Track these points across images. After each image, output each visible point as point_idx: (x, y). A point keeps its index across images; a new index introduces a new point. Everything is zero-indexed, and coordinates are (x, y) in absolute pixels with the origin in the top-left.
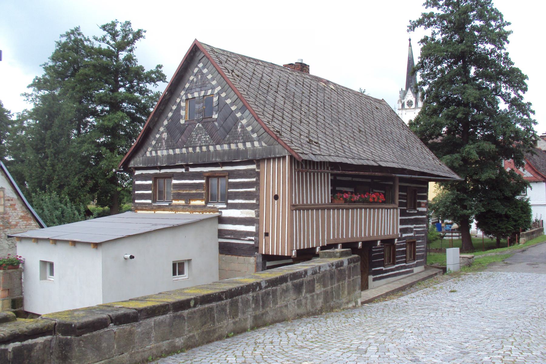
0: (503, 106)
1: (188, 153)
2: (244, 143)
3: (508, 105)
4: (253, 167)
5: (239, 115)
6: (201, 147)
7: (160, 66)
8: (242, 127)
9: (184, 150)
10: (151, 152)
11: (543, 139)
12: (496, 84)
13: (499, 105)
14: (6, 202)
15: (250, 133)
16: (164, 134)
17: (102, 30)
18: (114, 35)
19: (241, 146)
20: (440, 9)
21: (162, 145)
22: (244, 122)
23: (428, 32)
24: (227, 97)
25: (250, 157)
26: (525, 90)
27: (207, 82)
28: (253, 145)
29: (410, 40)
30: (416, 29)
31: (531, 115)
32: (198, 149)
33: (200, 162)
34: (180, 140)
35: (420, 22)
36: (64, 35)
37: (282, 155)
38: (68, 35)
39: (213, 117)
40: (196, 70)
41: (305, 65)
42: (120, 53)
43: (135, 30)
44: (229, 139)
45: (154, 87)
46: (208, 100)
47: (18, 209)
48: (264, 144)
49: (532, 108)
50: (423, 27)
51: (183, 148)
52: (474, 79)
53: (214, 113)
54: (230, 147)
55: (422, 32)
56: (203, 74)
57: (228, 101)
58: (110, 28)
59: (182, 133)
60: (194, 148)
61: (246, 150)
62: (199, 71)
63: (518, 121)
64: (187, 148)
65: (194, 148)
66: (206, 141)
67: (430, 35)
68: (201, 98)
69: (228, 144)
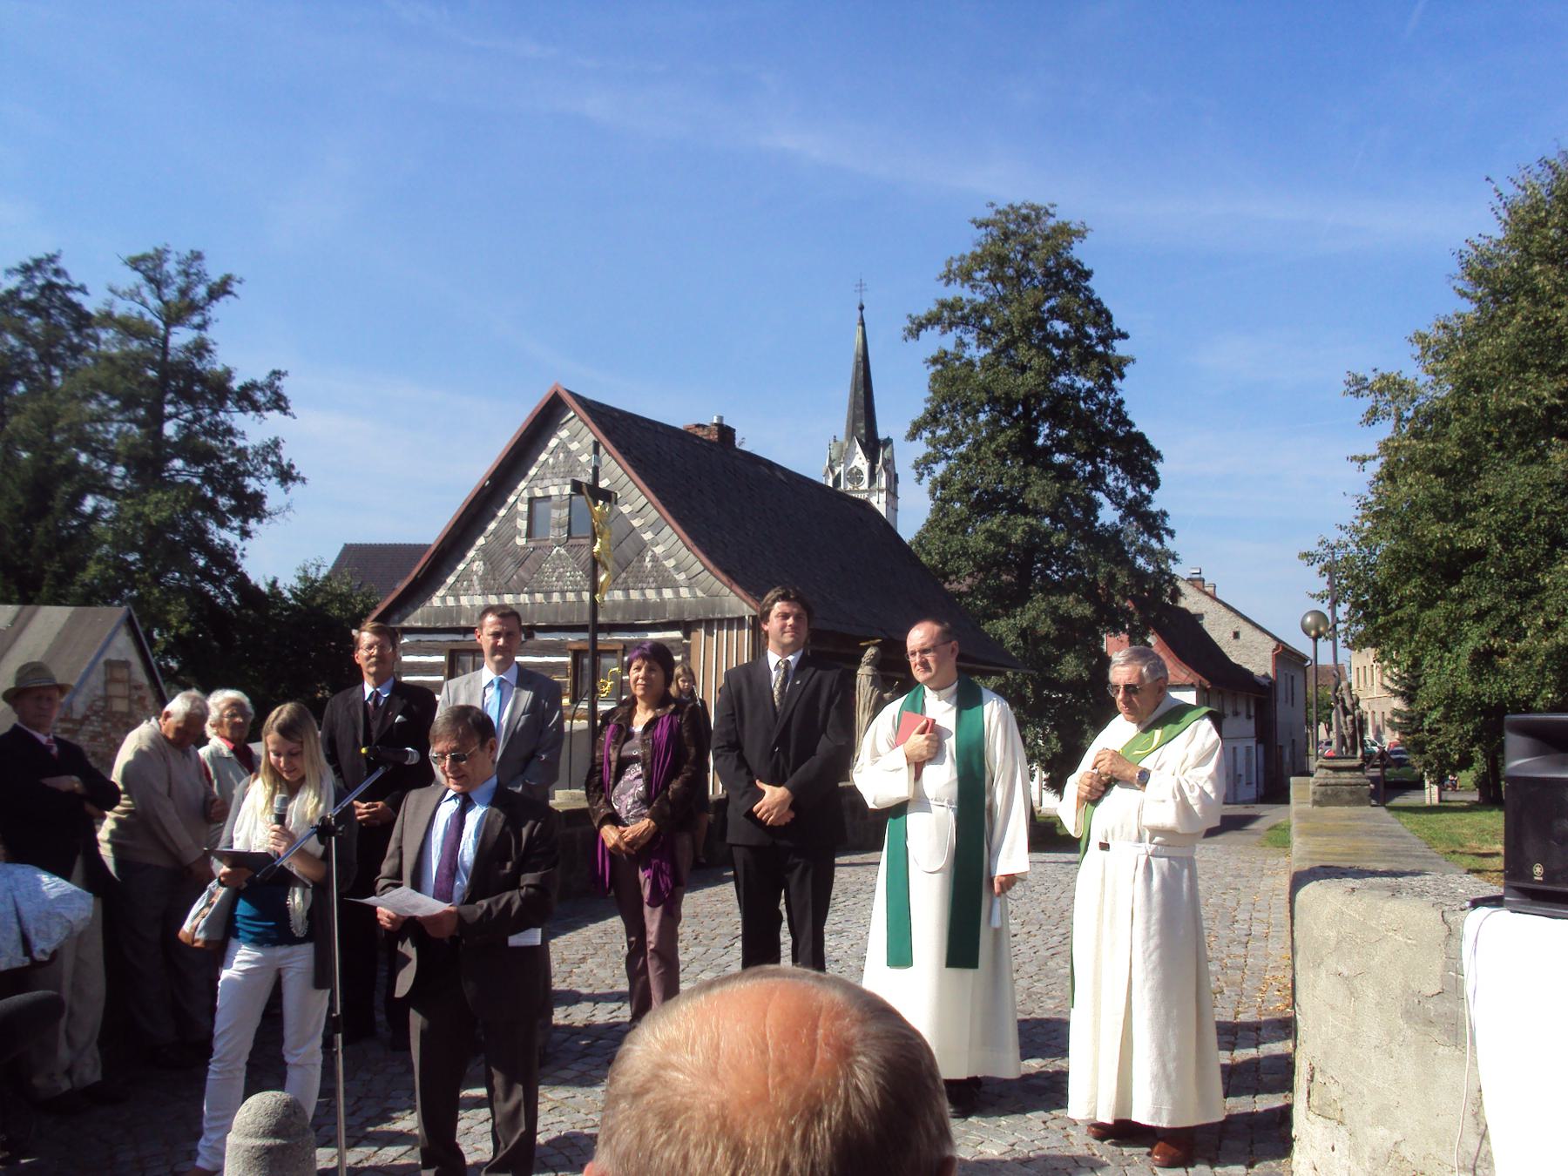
0: (1108, 515)
1: (533, 603)
2: (659, 589)
3: (1120, 512)
4: (677, 634)
5: (648, 536)
6: (563, 592)
7: (277, 374)
8: (655, 559)
9: (524, 598)
10: (443, 598)
11: (1194, 585)
12: (1094, 464)
13: (1100, 513)
14: (133, 691)
15: (673, 572)
16: (477, 563)
17: (128, 269)
18: (157, 283)
19: (651, 595)
21: (471, 585)
22: (659, 550)
23: (948, 342)
25: (669, 617)
26: (1154, 484)
27: (579, 469)
28: (677, 593)
29: (862, 308)
30: (923, 333)
31: (1166, 538)
32: (556, 597)
33: (561, 621)
34: (515, 577)
35: (932, 320)
36: (17, 270)
37: (736, 616)
38: (26, 270)
40: (553, 443)
42: (173, 329)
43: (215, 277)
45: (256, 422)
47: (150, 708)
48: (699, 594)
49: (1170, 524)
50: (938, 328)
51: (522, 592)
52: (1047, 452)
54: (628, 595)
56: (568, 452)
58: (149, 267)
59: (521, 563)
60: (548, 594)
61: (663, 603)
62: (561, 445)
64: (531, 593)
65: (548, 594)
66: (575, 581)
68: (564, 498)
69: (624, 590)
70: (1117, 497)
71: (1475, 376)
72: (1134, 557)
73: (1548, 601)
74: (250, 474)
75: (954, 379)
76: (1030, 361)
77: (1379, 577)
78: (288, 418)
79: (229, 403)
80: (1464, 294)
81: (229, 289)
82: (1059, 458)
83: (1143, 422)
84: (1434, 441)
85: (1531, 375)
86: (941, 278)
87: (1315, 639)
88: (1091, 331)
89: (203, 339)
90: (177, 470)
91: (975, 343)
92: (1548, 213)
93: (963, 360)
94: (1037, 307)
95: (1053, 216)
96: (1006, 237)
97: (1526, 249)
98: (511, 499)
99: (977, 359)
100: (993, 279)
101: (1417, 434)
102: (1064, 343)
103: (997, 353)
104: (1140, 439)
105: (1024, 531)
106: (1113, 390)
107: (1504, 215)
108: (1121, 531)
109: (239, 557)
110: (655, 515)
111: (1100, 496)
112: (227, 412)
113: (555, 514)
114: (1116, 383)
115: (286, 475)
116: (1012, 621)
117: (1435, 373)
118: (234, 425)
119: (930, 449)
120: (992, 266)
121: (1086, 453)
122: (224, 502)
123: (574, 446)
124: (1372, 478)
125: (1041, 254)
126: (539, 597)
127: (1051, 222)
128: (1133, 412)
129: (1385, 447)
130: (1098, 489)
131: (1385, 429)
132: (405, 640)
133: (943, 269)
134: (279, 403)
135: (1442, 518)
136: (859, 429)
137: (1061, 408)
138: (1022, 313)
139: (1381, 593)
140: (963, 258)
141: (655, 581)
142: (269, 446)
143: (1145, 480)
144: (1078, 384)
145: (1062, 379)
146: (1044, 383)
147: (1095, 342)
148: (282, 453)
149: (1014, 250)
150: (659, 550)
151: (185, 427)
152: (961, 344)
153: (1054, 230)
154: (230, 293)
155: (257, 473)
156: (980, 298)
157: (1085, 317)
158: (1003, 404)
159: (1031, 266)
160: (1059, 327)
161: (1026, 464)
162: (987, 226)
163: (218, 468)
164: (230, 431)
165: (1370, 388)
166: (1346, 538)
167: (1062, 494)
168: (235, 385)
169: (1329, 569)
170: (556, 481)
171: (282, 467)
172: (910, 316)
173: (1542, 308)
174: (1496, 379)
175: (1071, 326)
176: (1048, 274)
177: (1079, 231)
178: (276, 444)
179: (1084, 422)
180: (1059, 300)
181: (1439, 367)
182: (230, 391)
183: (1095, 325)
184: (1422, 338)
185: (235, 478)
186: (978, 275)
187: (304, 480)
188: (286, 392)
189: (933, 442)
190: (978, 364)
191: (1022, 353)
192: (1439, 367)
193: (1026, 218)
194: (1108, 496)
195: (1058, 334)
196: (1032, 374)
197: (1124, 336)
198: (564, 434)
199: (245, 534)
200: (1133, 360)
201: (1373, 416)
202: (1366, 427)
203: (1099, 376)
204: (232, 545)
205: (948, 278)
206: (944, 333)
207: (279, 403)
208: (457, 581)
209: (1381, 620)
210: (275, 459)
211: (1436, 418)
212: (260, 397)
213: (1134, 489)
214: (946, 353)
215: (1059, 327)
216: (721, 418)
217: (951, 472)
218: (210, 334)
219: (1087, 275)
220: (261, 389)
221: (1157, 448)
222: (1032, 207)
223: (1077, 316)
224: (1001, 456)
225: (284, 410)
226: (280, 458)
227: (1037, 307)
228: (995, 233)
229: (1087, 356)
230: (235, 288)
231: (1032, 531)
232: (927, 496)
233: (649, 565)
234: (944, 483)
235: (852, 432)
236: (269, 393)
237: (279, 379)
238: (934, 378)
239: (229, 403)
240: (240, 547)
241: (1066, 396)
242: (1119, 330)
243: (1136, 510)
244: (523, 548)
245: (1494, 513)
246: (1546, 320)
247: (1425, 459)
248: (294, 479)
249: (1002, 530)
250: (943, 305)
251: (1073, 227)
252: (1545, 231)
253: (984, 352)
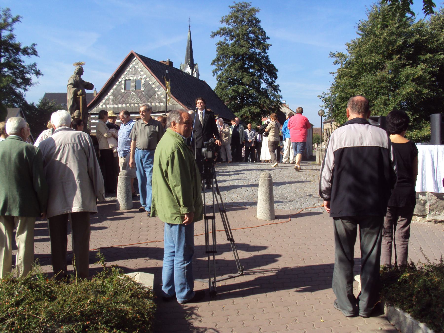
0: (264, 86)
2: (159, 103)
5: (156, 90)
6: (134, 104)
7: (34, 45)
8: (158, 95)
9: (124, 105)
13: (261, 85)
19: (157, 104)
20: (230, 25)
22: (159, 93)
24: (150, 81)
26: (276, 78)
29: (190, 27)
30: (215, 36)
31: (279, 92)
32: (132, 105)
33: (134, 111)
35: (218, 33)
39: (142, 89)
40: (131, 66)
41: (171, 62)
43: (14, 16)
44: (151, 101)
46: (138, 82)
49: (280, 88)
50: (219, 35)
52: (248, 68)
53: (142, 88)
55: (219, 39)
56: (135, 68)
57: (151, 83)
60: (130, 104)
63: (273, 95)
64: (126, 104)
65: (130, 104)
67: (223, 40)
70: (266, 81)
71: (360, 54)
72: (271, 97)
73: (375, 108)
74: (27, 73)
75: (224, 49)
76: (244, 44)
77: (337, 102)
78: (38, 57)
79: (20, 53)
80: (359, 34)
81: (19, 20)
82: (251, 70)
83: (273, 61)
84: (350, 69)
85: (374, 55)
86: (220, 22)
87: (321, 116)
88: (260, 37)
89: (12, 34)
90: (5, 72)
91: (229, 39)
92: (379, 15)
93: (226, 44)
94: (246, 30)
95: (251, 6)
96: (238, 11)
97: (373, 24)
98: (120, 80)
99: (230, 44)
100: (234, 22)
101: (346, 68)
102: (254, 40)
103: (235, 42)
104: (272, 65)
105: (242, 90)
106: (266, 53)
107: (369, 15)
108: (267, 90)
109: (24, 96)
110: (158, 84)
111: (262, 81)
112: (19, 55)
113: (132, 84)
114: (267, 51)
115: (38, 73)
116: (239, 113)
117: (351, 53)
118: (21, 59)
119: (217, 67)
120: (234, 18)
121: (259, 69)
122: (19, 81)
123: (137, 67)
124: (335, 78)
125: (248, 16)
126: (128, 105)
127: (250, 7)
128: (271, 59)
129: (339, 70)
130: (261, 79)
131: (339, 66)
132: (92, 116)
133: (221, 19)
134: (35, 53)
135: (352, 88)
136: (189, 61)
137: (252, 57)
138: (242, 32)
139: (337, 106)
140: (226, 16)
141: (158, 101)
142: (33, 65)
143: (274, 77)
144: (256, 51)
145: (253, 50)
146: (248, 51)
147: (261, 40)
148: (37, 67)
149: (240, 15)
150: (159, 93)
151: (7, 59)
152: (225, 39)
153: (251, 10)
154: (19, 21)
155: (29, 73)
156: (231, 27)
157: (258, 33)
158: (237, 56)
159: (244, 19)
160: (252, 35)
161: (243, 72)
162: (233, 8)
163: (18, 71)
164: (20, 61)
165: (335, 56)
166: (329, 92)
167: (253, 80)
168: (22, 47)
169: (325, 100)
170: (132, 75)
171: (37, 71)
172: (212, 32)
173: (377, 39)
174: (365, 56)
175: (255, 35)
176: (249, 21)
177: (257, 10)
178: (35, 65)
179: (258, 60)
180: (251, 28)
181: (352, 52)
182: (20, 49)
183: (261, 35)
184: (348, 44)
185: (23, 74)
186: (230, 21)
187: (43, 75)
188: (36, 50)
189: (218, 66)
190: (230, 45)
191: (242, 42)
192: (352, 52)
193: (243, 6)
194: (264, 81)
195: (251, 38)
196: (245, 48)
197: (269, 38)
198: (134, 63)
199: (25, 90)
200: (272, 45)
201: (336, 62)
202: (334, 65)
203: (262, 49)
204: (22, 93)
205: (222, 22)
206: (221, 36)
207: (35, 53)
208: (106, 101)
209: (337, 112)
210: (35, 69)
211: (350, 64)
212: (29, 51)
213: (271, 79)
214: (221, 42)
215: (252, 35)
216: (169, 59)
217: (223, 73)
218: (14, 32)
219: (259, 22)
220: (29, 49)
221: (277, 68)
222: (245, 3)
223: (257, 33)
224: (236, 70)
225: (36, 55)
226: (36, 68)
227: (246, 30)
228: (235, 10)
229: (259, 43)
230: (20, 19)
231: (245, 89)
232: (216, 80)
233: (157, 97)
234: (220, 77)
235: (187, 62)
236: (32, 50)
237: (35, 46)
238: (218, 48)
239: (20, 53)
240: (24, 93)
241: (253, 54)
242: (267, 37)
243: (271, 84)
244: (123, 92)
245: (364, 87)
246: (377, 41)
247: (349, 74)
248: (40, 74)
249: (236, 89)
250: (221, 29)
251: (256, 9)
252: (378, 19)
253: (232, 42)
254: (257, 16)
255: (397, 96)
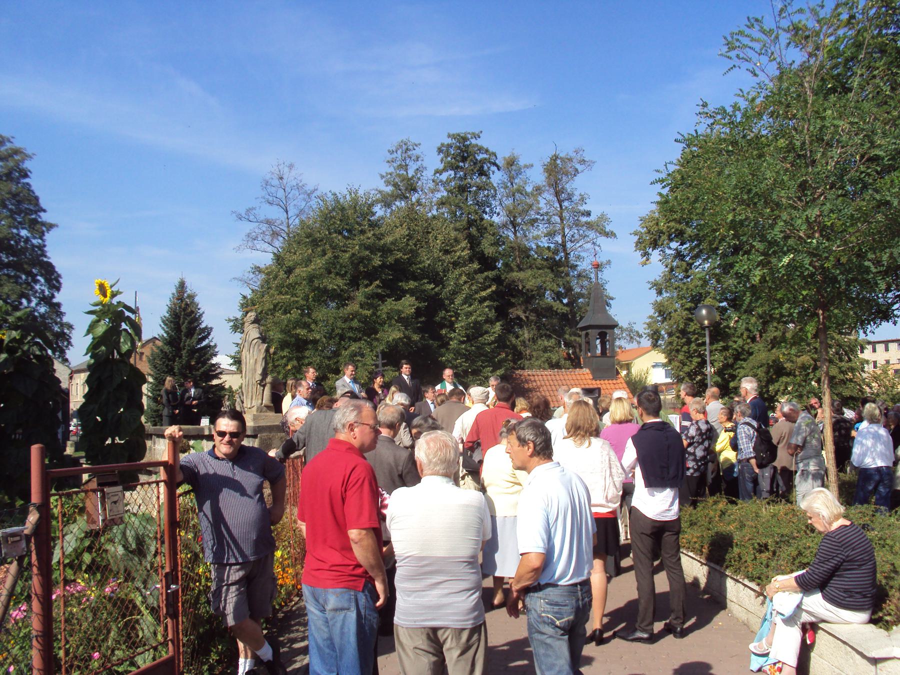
26: (58, 289)
200: (57, 226)
254: (27, 165)
255: (375, 343)
